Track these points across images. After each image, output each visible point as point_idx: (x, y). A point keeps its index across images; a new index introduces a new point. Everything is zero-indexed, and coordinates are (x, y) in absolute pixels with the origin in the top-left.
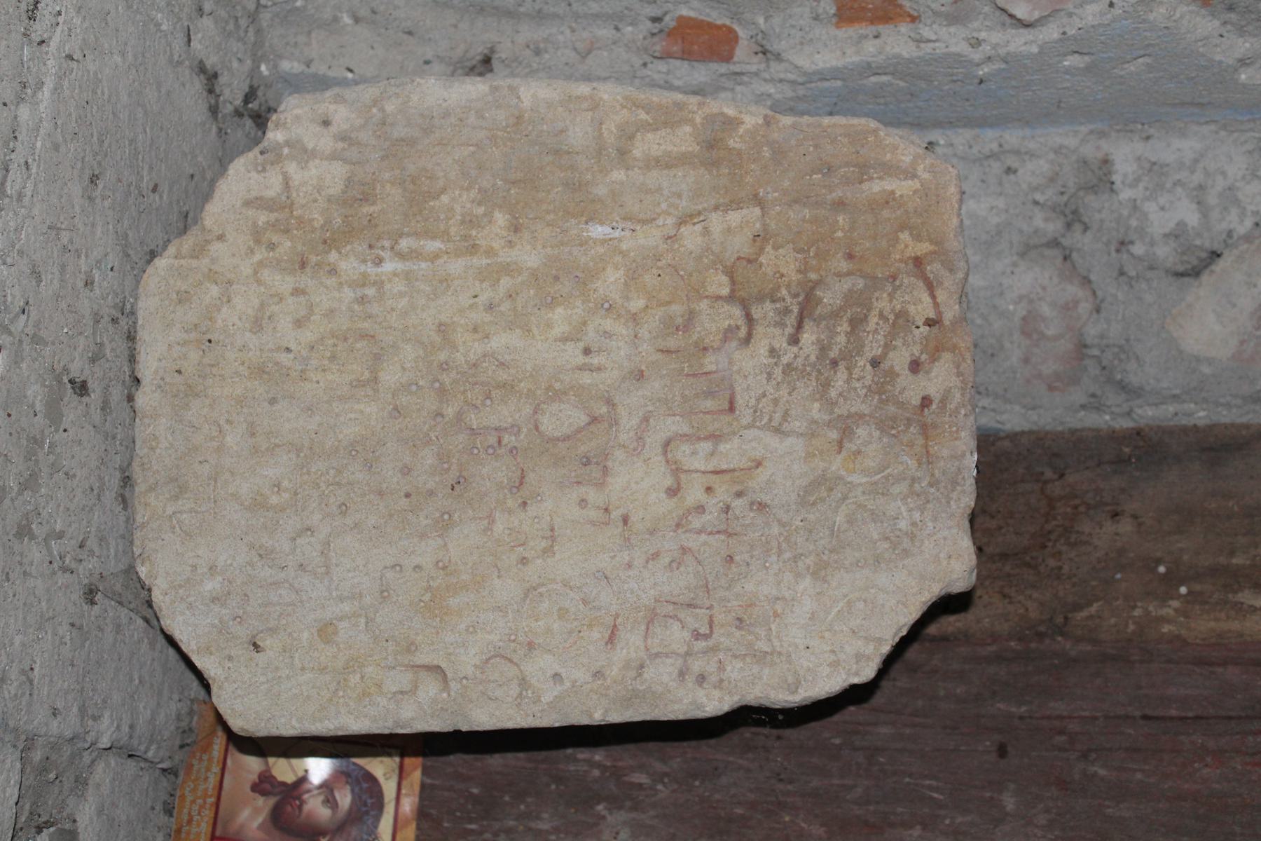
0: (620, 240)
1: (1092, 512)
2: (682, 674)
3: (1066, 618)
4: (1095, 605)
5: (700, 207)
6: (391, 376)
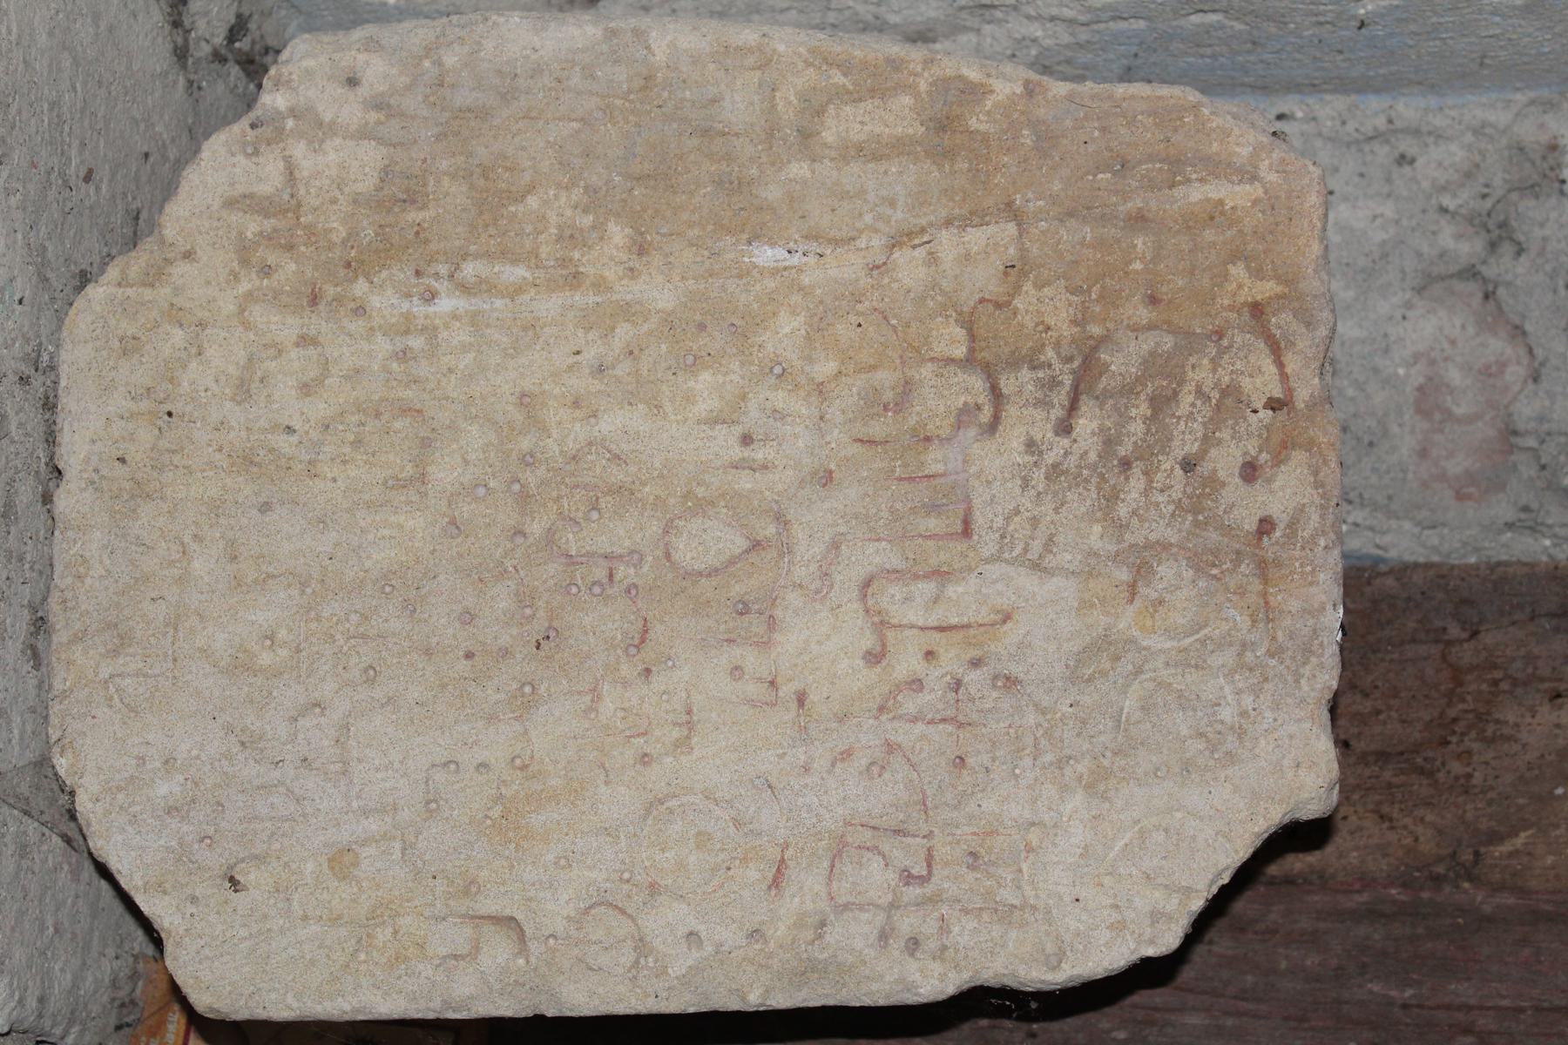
0: (800, 270)
1: (1519, 691)
2: (884, 937)
3: (1477, 854)
4: (1523, 835)
5: (924, 222)
6: (445, 472)
